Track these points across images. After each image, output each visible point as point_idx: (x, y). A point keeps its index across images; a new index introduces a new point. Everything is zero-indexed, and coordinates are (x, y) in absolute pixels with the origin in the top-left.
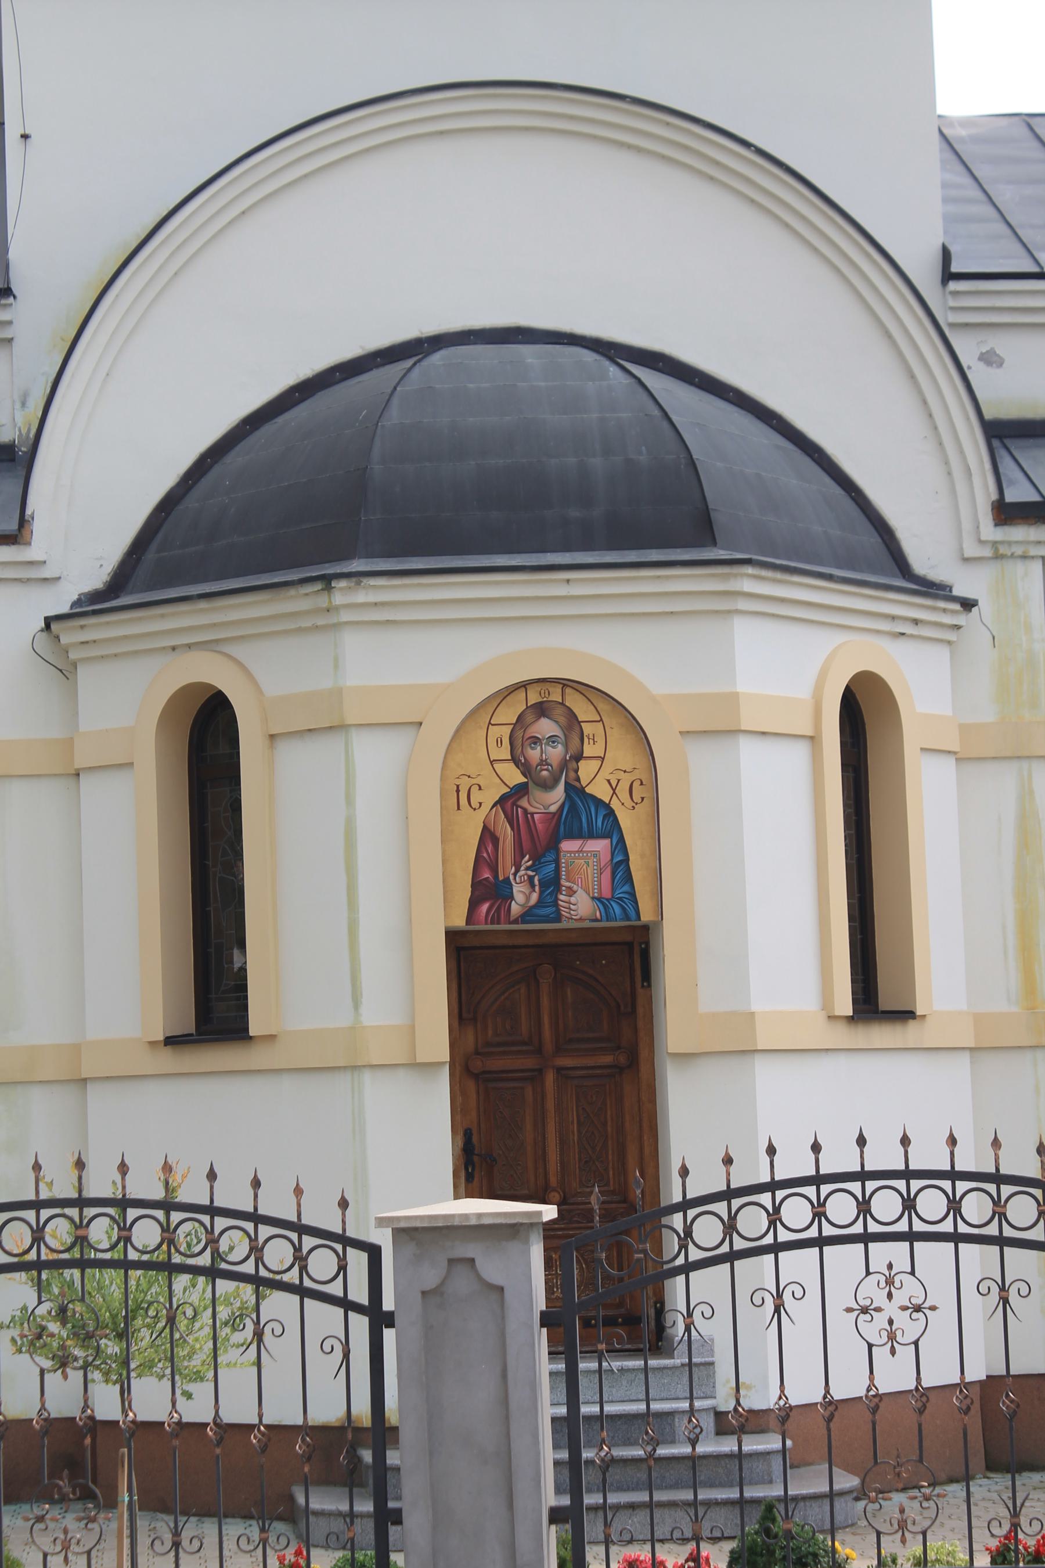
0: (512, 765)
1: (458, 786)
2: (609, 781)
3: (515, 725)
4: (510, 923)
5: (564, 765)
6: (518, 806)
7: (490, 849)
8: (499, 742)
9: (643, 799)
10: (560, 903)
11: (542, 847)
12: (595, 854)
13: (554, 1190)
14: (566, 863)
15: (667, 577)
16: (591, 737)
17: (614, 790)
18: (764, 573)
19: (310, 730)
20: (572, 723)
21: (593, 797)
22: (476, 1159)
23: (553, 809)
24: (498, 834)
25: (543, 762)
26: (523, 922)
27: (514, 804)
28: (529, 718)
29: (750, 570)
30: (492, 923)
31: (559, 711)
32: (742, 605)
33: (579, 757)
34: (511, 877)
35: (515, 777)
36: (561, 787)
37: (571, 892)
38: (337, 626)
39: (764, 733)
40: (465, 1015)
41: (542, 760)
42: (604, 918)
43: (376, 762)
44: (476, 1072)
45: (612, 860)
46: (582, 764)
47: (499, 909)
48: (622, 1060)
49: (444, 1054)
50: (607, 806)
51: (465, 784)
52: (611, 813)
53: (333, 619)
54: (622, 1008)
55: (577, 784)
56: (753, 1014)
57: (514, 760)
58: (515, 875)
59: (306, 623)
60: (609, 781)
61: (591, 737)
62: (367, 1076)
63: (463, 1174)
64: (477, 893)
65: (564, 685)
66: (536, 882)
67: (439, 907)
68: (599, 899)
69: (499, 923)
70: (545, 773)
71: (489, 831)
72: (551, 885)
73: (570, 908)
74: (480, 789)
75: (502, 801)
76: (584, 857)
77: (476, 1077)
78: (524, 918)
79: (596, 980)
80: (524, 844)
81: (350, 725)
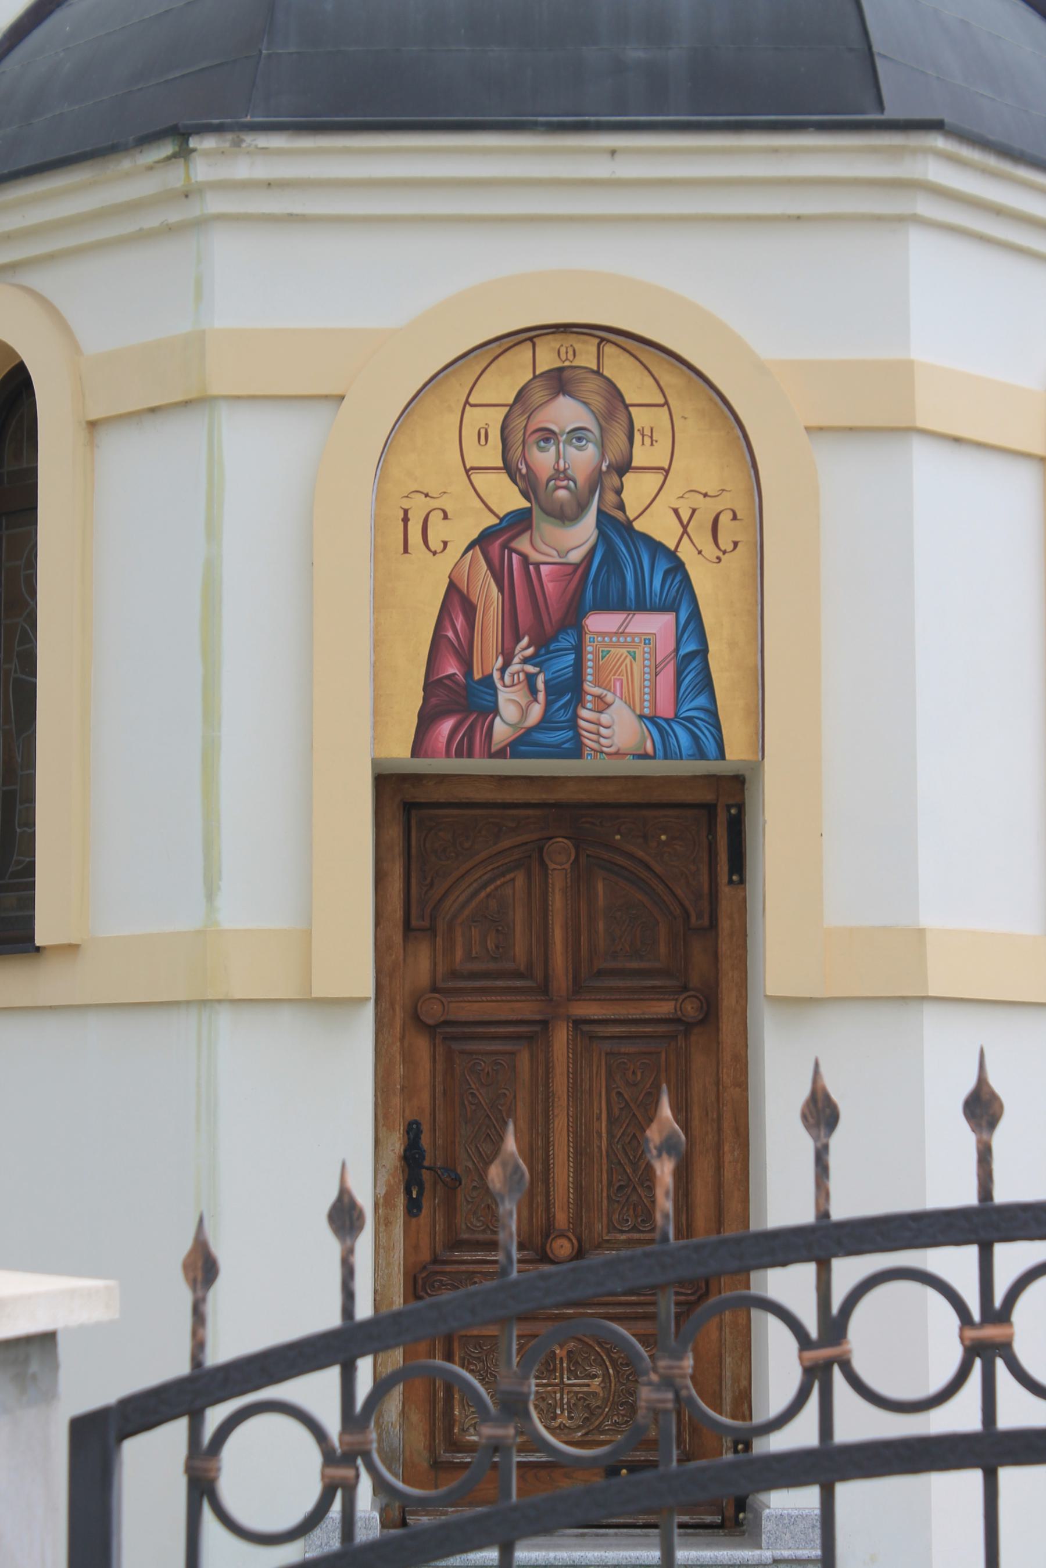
0: (504, 477)
1: (406, 512)
2: (676, 511)
3: (512, 406)
4: (492, 756)
5: (597, 480)
6: (512, 550)
7: (460, 622)
8: (483, 436)
9: (736, 544)
10: (582, 723)
11: (554, 627)
12: (648, 640)
13: (562, 1235)
14: (595, 653)
15: (791, 151)
16: (647, 432)
17: (685, 528)
18: (966, 152)
19: (153, 410)
20: (615, 405)
21: (647, 539)
22: (426, 1175)
23: (575, 556)
24: (474, 599)
25: (560, 474)
26: (515, 755)
27: (505, 546)
28: (538, 395)
29: (939, 142)
30: (459, 754)
31: (591, 386)
32: (925, 207)
33: (624, 467)
34: (496, 675)
35: (509, 499)
36: (590, 518)
37: (602, 705)
38: (202, 223)
39: (957, 440)
40: (414, 923)
41: (557, 470)
42: (660, 753)
43: (263, 461)
44: (431, 1022)
45: (677, 650)
46: (629, 479)
47: (470, 733)
48: (691, 1009)
49: (362, 980)
50: (672, 555)
51: (418, 508)
52: (677, 568)
53: (193, 210)
54: (693, 919)
55: (618, 514)
56: (921, 932)
57: (509, 468)
58: (503, 670)
59: (151, 221)
60: (676, 511)
61: (647, 432)
62: (224, 1019)
63: (400, 1201)
64: (434, 701)
65: (602, 339)
66: (540, 685)
67: (368, 723)
68: (652, 719)
69: (470, 755)
70: (562, 493)
71: (459, 591)
72: (568, 691)
73: (598, 734)
74: (446, 517)
75: (483, 540)
76: (629, 645)
77: (431, 1030)
78: (518, 747)
79: (648, 868)
80: (520, 619)
81: (215, 398)
